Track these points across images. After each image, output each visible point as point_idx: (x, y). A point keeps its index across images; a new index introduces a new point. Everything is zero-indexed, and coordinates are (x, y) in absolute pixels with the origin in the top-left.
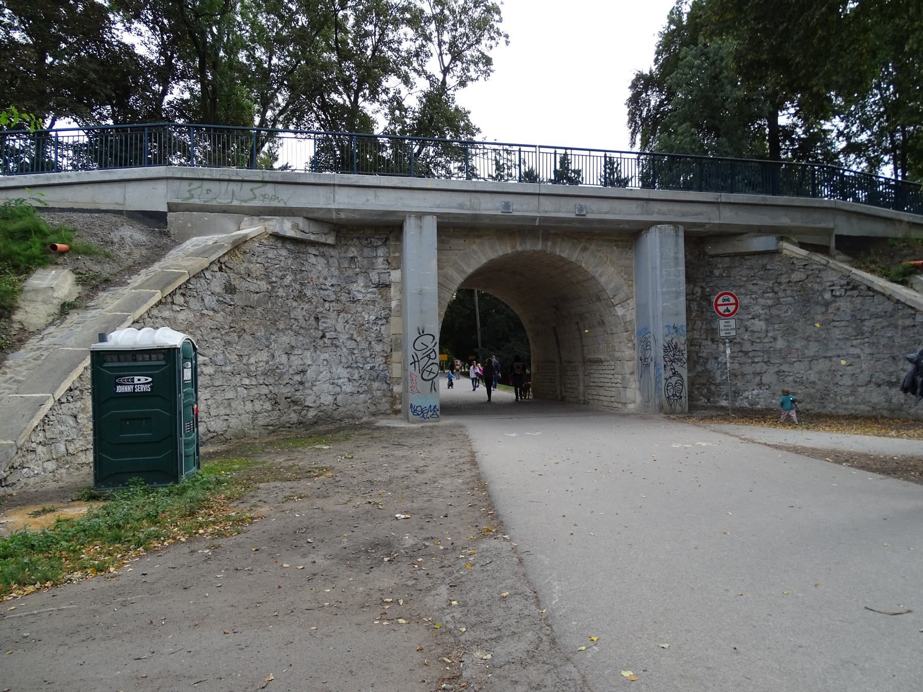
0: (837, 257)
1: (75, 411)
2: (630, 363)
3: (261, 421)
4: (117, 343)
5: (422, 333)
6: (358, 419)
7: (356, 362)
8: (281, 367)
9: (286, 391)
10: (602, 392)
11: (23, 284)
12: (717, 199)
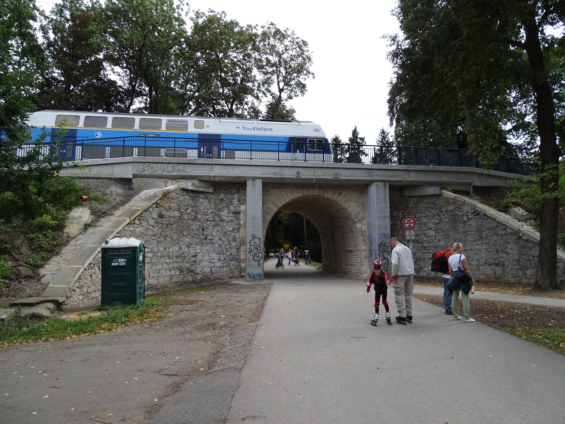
0: (474, 197)
1: (91, 274)
2: (365, 252)
3: (174, 280)
4: (112, 245)
5: (254, 237)
6: (223, 280)
7: (223, 251)
8: (185, 254)
9: (187, 265)
10: (352, 268)
11: (68, 215)
12: (408, 168)
